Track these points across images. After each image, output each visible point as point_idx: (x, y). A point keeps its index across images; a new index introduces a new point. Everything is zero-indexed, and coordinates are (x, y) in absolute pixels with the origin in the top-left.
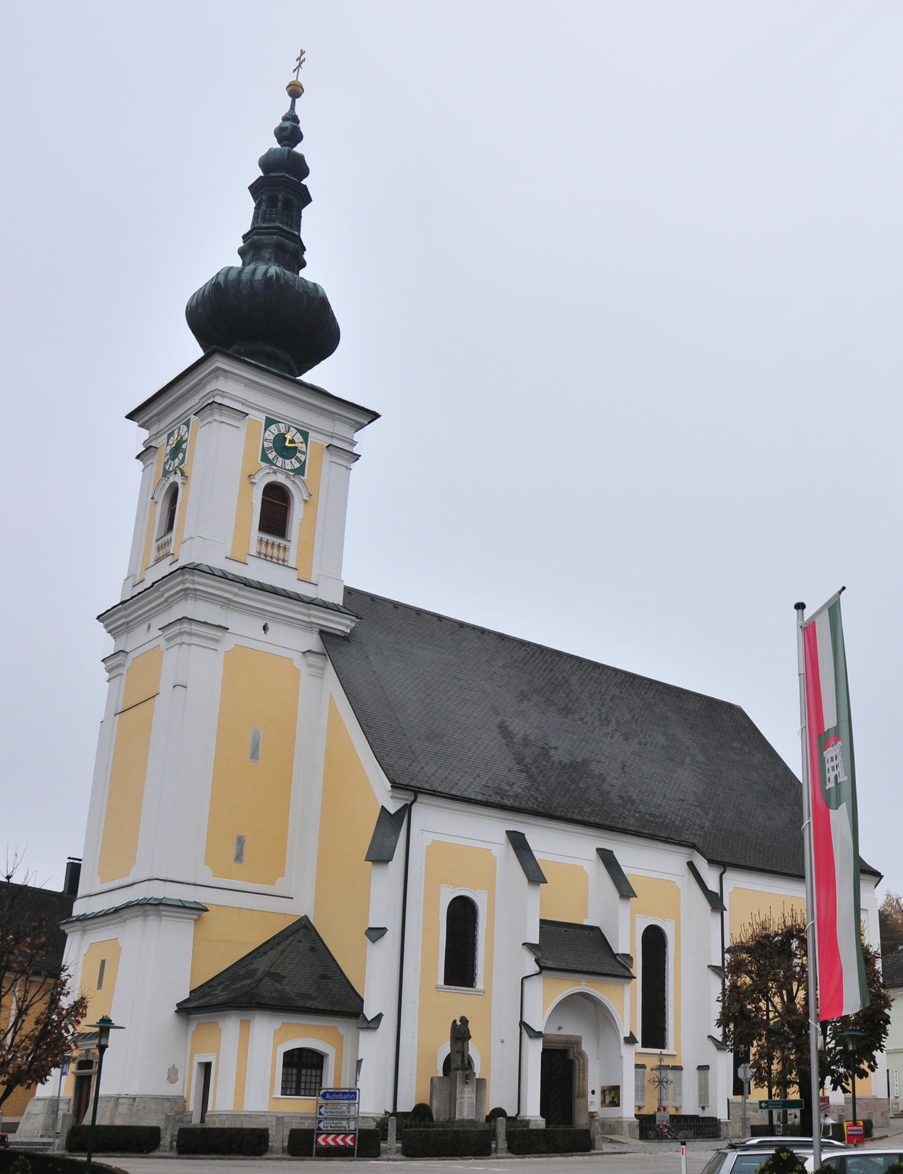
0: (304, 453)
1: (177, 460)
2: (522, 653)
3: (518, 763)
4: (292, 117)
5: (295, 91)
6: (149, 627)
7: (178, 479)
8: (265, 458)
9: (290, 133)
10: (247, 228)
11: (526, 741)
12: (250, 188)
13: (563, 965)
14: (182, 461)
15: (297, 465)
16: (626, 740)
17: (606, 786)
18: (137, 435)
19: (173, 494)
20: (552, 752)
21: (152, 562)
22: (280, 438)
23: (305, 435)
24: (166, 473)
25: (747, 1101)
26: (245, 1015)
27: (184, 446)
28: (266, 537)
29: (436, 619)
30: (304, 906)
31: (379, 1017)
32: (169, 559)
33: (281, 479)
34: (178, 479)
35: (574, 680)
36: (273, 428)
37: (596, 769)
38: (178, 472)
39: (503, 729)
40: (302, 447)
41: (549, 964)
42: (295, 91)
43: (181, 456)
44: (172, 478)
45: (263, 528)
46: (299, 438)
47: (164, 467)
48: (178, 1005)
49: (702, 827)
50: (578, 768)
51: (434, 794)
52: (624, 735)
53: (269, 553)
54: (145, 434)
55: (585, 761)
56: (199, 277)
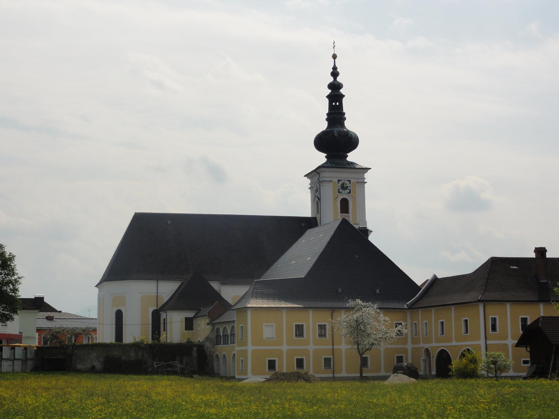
4: (335, 68)
5: (334, 57)
8: (339, 192)
13: (88, 320)
15: (348, 191)
19: (319, 199)
22: (343, 184)
23: (350, 181)
26: (157, 280)
28: (342, 214)
33: (345, 196)
36: (340, 182)
40: (349, 185)
42: (334, 57)
45: (341, 212)
46: (348, 183)
48: (12, 258)
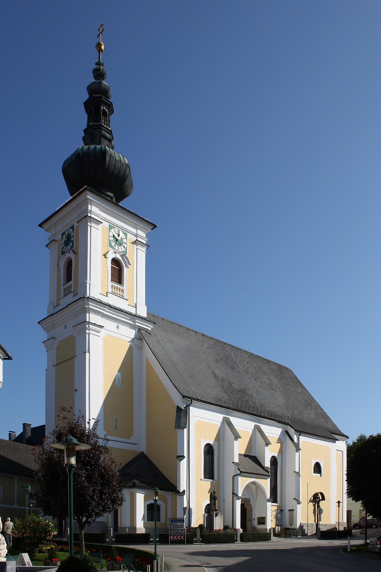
0: (126, 244)
1: (69, 246)
2: (212, 342)
3: (223, 389)
6: (66, 326)
7: (72, 255)
9: (99, 74)
10: (85, 126)
11: (223, 380)
12: (84, 104)
14: (73, 246)
16: (256, 380)
17: (254, 400)
18: (44, 236)
20: (233, 385)
21: (62, 296)
24: (63, 253)
25: (321, 523)
27: (72, 239)
29: (178, 326)
30: (143, 448)
31: (184, 491)
32: (72, 294)
34: (72, 255)
35: (232, 354)
37: (249, 392)
38: (71, 252)
39: (214, 374)
41: (243, 471)
43: (71, 244)
44: (68, 255)
47: (62, 250)
49: (288, 417)
50: (243, 392)
51: (198, 400)
52: (254, 378)
53: (116, 292)
54: (49, 235)
55: (244, 389)
56: (68, 152)
